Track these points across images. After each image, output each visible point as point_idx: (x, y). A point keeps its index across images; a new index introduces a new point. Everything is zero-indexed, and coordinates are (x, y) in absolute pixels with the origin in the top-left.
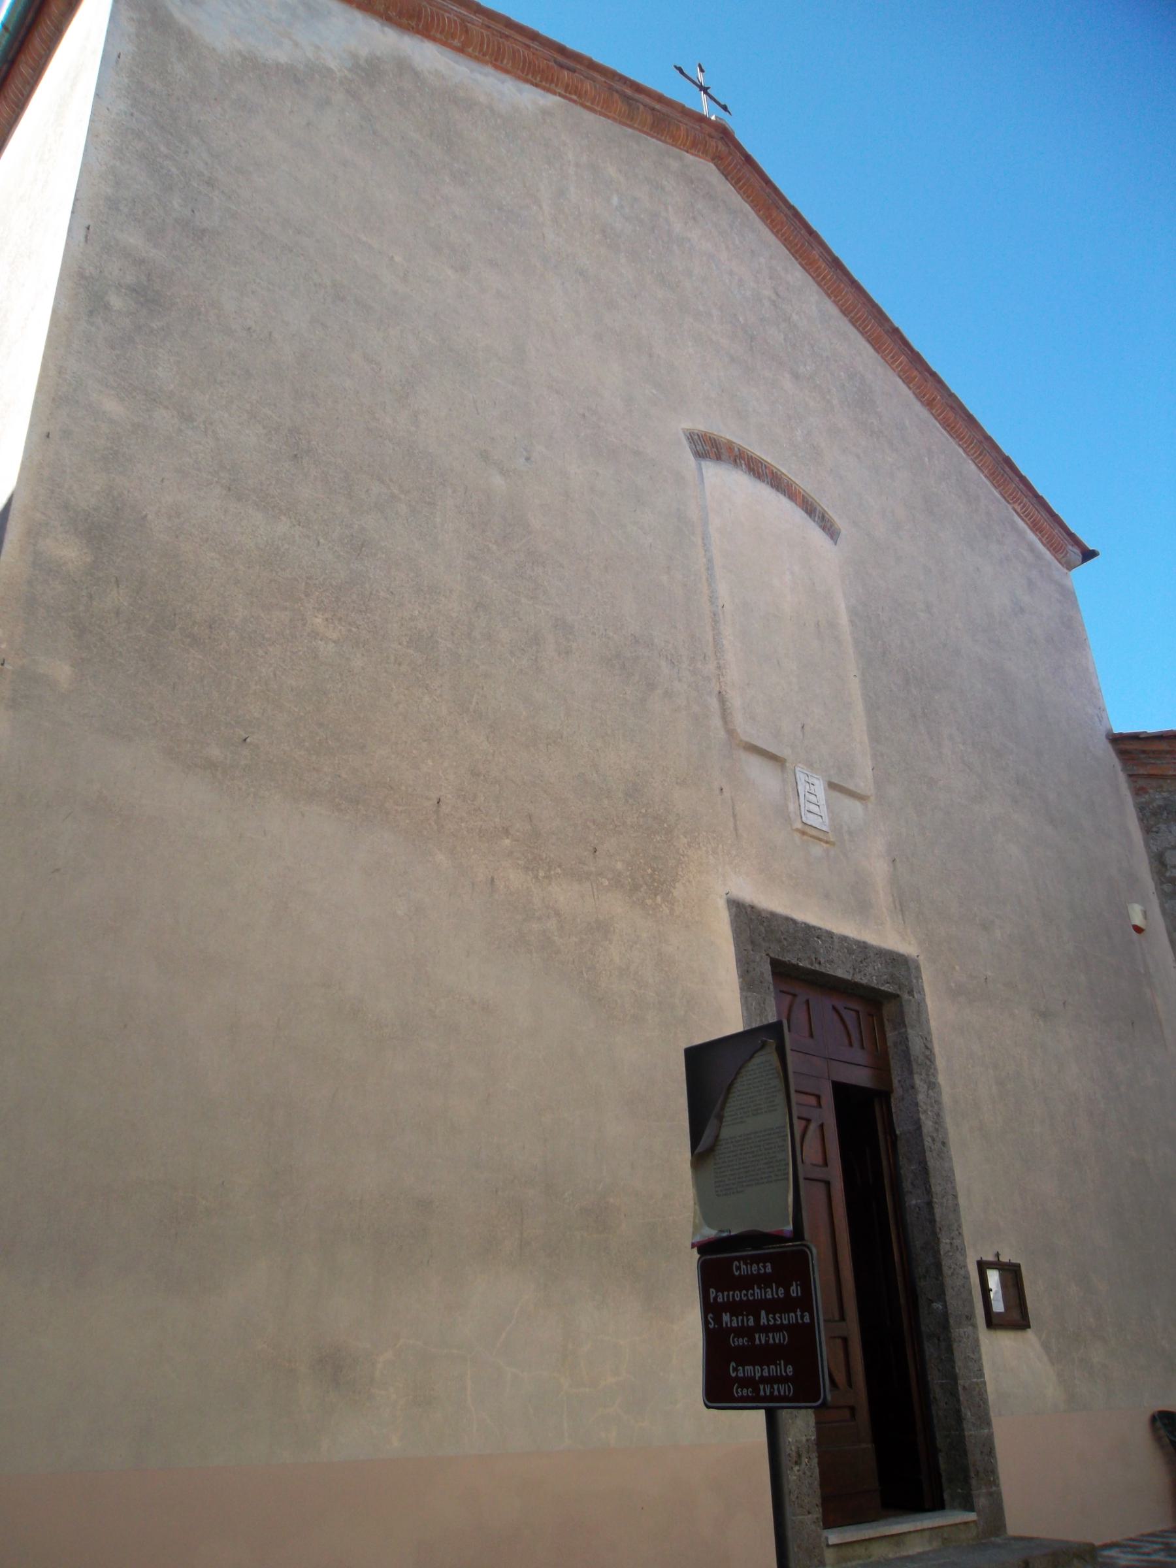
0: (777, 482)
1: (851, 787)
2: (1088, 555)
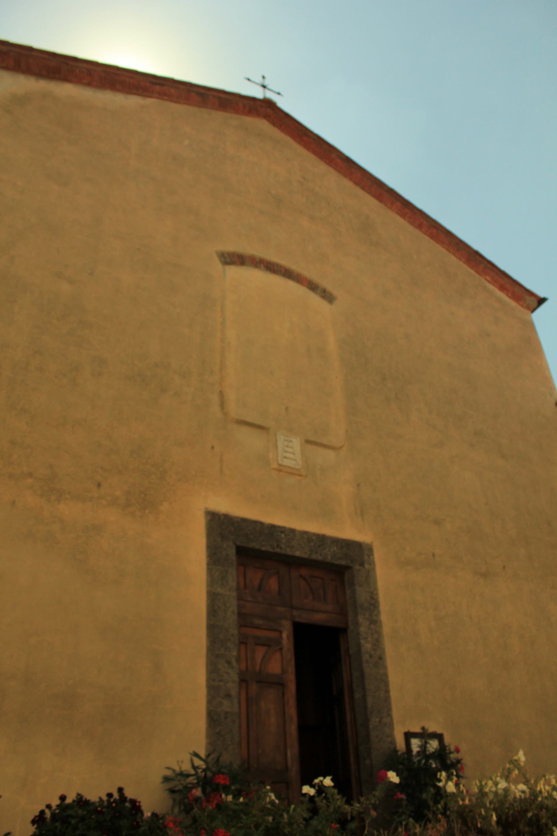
0: (288, 274)
1: (325, 442)
2: (541, 301)
